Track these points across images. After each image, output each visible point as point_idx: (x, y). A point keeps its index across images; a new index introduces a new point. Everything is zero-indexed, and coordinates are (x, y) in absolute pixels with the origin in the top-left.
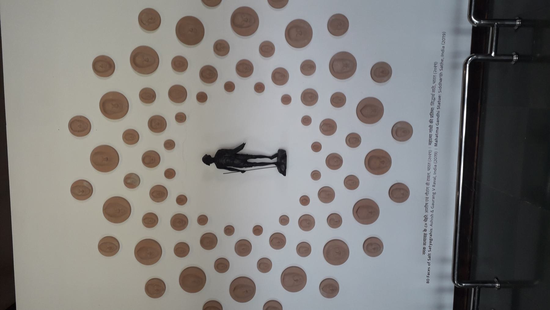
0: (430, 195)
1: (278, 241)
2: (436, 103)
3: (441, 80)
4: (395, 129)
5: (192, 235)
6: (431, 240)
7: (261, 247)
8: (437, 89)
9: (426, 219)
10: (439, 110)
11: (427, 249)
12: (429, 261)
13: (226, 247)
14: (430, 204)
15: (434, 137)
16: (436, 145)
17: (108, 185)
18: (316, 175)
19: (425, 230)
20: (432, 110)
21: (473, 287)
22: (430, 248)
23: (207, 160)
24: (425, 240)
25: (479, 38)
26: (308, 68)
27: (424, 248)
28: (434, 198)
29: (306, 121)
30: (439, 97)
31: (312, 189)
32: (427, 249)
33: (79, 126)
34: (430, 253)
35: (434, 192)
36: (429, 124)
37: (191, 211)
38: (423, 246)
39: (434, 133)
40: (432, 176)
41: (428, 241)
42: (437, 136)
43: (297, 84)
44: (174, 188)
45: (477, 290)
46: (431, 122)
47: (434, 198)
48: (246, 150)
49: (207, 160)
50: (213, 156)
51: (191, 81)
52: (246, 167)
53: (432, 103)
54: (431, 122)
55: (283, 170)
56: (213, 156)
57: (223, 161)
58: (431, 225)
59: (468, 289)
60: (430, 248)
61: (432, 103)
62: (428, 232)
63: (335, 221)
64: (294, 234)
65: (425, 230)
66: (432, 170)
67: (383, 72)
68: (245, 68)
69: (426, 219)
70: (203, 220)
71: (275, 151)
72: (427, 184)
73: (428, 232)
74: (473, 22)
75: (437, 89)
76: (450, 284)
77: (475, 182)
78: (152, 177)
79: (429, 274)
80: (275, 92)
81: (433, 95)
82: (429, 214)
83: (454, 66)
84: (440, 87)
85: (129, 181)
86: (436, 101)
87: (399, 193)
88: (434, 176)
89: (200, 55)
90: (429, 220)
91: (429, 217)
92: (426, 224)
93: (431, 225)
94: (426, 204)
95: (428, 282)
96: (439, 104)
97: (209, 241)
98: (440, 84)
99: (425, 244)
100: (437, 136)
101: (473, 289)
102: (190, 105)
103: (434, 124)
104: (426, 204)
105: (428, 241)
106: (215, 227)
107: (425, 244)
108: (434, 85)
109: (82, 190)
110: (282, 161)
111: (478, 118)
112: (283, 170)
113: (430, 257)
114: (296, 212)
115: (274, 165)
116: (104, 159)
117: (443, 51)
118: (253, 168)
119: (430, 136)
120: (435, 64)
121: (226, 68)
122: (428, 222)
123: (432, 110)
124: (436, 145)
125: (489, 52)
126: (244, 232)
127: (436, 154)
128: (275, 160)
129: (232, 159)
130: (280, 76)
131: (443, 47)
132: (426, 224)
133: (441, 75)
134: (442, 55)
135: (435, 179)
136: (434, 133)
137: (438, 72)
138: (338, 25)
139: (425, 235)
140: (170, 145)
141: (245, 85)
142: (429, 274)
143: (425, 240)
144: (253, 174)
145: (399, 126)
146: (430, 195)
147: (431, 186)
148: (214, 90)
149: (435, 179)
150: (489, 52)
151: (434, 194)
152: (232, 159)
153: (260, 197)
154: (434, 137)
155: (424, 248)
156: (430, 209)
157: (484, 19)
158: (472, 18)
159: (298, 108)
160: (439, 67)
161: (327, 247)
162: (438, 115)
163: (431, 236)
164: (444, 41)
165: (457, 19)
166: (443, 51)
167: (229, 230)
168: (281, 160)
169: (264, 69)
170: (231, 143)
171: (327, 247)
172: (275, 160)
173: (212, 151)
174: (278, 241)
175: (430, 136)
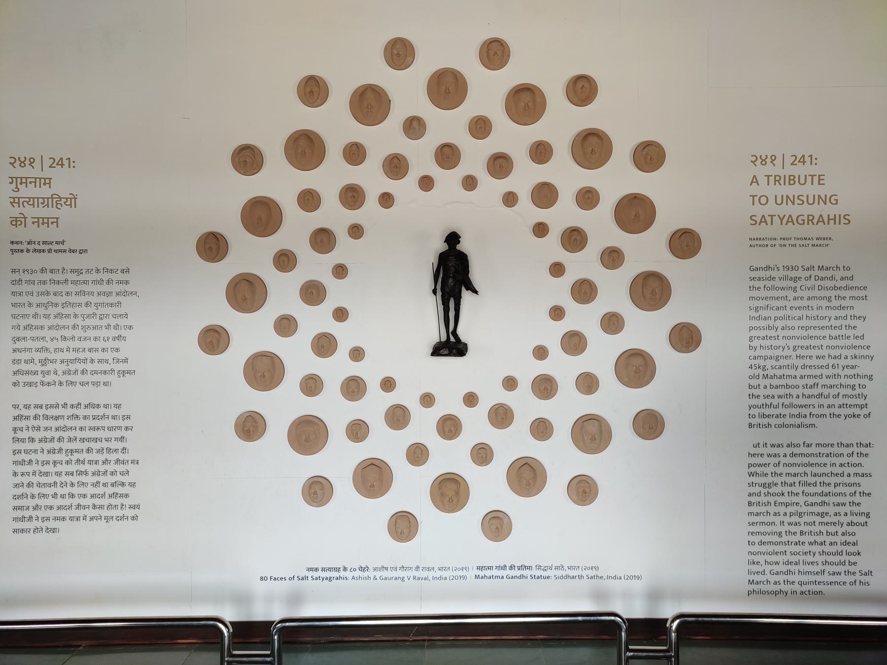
0: (400, 574)
1: (324, 345)
2: (538, 573)
3: (573, 577)
4: (501, 515)
5: (332, 214)
6: (330, 579)
7: (314, 320)
8: (559, 573)
9: (362, 569)
10: (529, 577)
11: (316, 574)
12: (296, 578)
13: (313, 266)
14: (385, 574)
15: (488, 573)
16: (477, 577)
17: (408, 91)
18: (471, 400)
19: (345, 569)
20: (529, 568)
21: (273, 652)
22: (317, 579)
23: (453, 239)
24: (330, 569)
25: (652, 628)
26: (588, 383)
27: (317, 570)
28: (396, 579)
29: (510, 383)
30: (548, 577)
31: (406, 395)
32: (316, 574)
33: (495, 53)
34: (310, 578)
35: (406, 579)
36: (508, 565)
37: (369, 212)
38: (320, 567)
39: (495, 572)
40: (431, 574)
41: (328, 574)
42: (490, 578)
43: (564, 368)
44: (405, 188)
45: (269, 659)
46: (512, 567)
47: (396, 579)
48: (466, 295)
49: (453, 239)
50: (459, 247)
51: (564, 214)
52: (442, 296)
53: (539, 567)
54: (512, 567)
55: (438, 350)
56: (459, 247)
57: (452, 262)
58: (353, 578)
59: (268, 644)
60: (317, 579)
61: (539, 567)
62: (342, 574)
63: (357, 431)
64: (335, 369)
65: (345, 569)
66: (438, 574)
67: (585, 492)
68: (584, 291)
69: (362, 569)
70: (356, 231)
71: (463, 337)
72: (418, 567)
73: (342, 574)
74: (673, 621)
75: (559, 573)
76: (275, 613)
77: (424, 640)
78: (420, 155)
79: (275, 579)
80: (552, 334)
81: (551, 568)
82: (371, 574)
83: (599, 595)
84: (562, 577)
85: (415, 123)
86: (537, 573)
87: (403, 526)
88: (430, 578)
89: (601, 227)
90: (361, 574)
91: (366, 574)
92: (355, 570)
93: (353, 578)
94: (387, 569)
95: (262, 579)
96: (538, 578)
97: (323, 240)
98: (567, 577)
99: (323, 569)
100: (490, 578)
101: (269, 652)
102: (529, 212)
103: (508, 572)
104: (387, 569)
105: (328, 574)
106: (345, 249)
107: (323, 569)
108: (566, 568)
109: (399, 53)
110: (454, 351)
111: (521, 637)
112: (438, 350)
113: (303, 579)
114: (370, 372)
115: (444, 338)
116: (447, 88)
117: (615, 577)
118: (441, 307)
119: (490, 568)
120: (597, 568)
121: (584, 264)
122: (358, 573)
123: (529, 568)
124: (477, 577)
125: (631, 647)
126: (337, 293)
127: (464, 577)
128: (452, 339)
129: (453, 274)
130: (574, 343)
131: (621, 578)
132: (355, 570)
133: (581, 577)
134: (609, 577)
135: (426, 579)
136: (495, 572)
137: (584, 573)
138: (250, 427)
139: (337, 570)
140: (470, 183)
141: (560, 291)
142: (275, 579)
143: (330, 569)
144: (429, 308)
145: (506, 520)
146: (400, 574)
147: (413, 573)
148: (552, 248)
149: (426, 579)
150: (631, 647)
151: (403, 579)
152: (453, 274)
153: (395, 317)
154: (488, 573)
155: (317, 570)
156: (378, 574)
157: (678, 637)
158: (678, 621)
159: (528, 370)
160: (591, 573)
161: (317, 420)
162: (522, 577)
163: (337, 579)
164: (630, 578)
165: (678, 595)
166: (615, 577)
167: (340, 271)
168: (451, 347)
169: (584, 318)
170: (476, 274)
171: (317, 420)
172: (452, 339)
173: (464, 246)
174: (324, 345)
175: (490, 568)
